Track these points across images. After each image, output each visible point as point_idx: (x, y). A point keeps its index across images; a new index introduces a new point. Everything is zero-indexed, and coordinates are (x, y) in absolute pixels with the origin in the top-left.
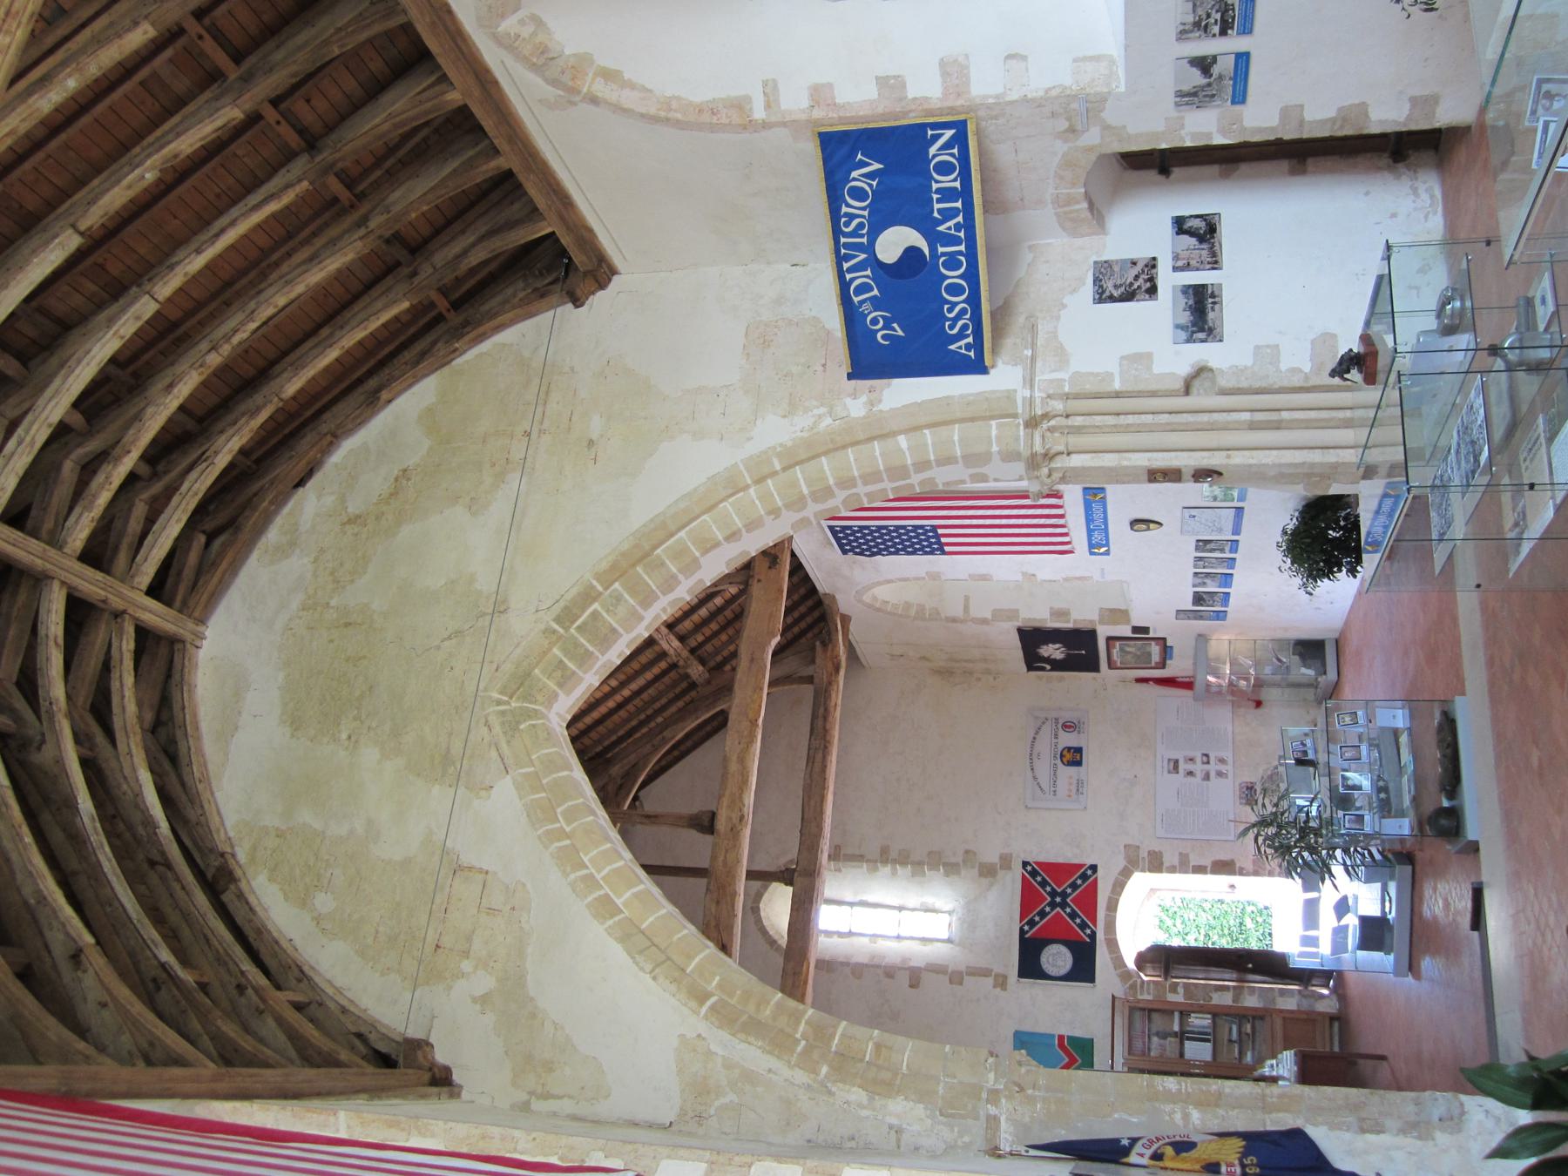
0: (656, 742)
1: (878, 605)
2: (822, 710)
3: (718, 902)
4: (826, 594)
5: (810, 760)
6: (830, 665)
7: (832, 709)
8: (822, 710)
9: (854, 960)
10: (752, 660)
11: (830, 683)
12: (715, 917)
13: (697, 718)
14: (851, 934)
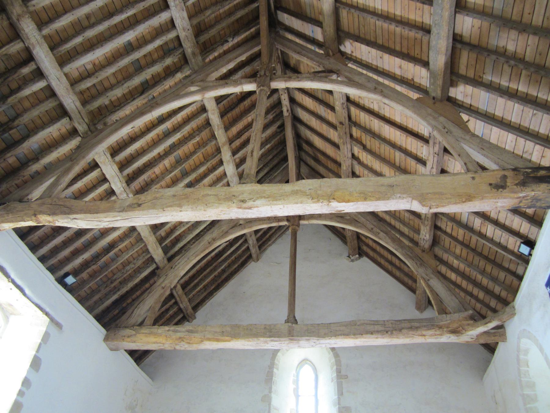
0: (376, 230)
1: (522, 357)
2: (417, 324)
3: (174, 196)
4: (514, 307)
5: (375, 323)
6: (455, 325)
7: (419, 332)
8: (417, 324)
9: (273, 396)
10: (391, 186)
11: (440, 327)
12: (163, 196)
13: (396, 250)
14: (297, 396)
